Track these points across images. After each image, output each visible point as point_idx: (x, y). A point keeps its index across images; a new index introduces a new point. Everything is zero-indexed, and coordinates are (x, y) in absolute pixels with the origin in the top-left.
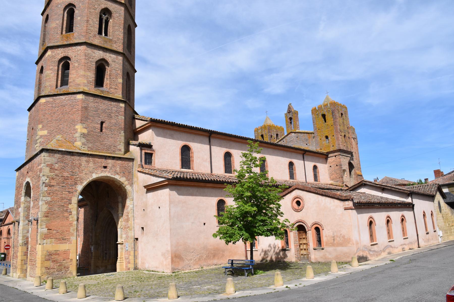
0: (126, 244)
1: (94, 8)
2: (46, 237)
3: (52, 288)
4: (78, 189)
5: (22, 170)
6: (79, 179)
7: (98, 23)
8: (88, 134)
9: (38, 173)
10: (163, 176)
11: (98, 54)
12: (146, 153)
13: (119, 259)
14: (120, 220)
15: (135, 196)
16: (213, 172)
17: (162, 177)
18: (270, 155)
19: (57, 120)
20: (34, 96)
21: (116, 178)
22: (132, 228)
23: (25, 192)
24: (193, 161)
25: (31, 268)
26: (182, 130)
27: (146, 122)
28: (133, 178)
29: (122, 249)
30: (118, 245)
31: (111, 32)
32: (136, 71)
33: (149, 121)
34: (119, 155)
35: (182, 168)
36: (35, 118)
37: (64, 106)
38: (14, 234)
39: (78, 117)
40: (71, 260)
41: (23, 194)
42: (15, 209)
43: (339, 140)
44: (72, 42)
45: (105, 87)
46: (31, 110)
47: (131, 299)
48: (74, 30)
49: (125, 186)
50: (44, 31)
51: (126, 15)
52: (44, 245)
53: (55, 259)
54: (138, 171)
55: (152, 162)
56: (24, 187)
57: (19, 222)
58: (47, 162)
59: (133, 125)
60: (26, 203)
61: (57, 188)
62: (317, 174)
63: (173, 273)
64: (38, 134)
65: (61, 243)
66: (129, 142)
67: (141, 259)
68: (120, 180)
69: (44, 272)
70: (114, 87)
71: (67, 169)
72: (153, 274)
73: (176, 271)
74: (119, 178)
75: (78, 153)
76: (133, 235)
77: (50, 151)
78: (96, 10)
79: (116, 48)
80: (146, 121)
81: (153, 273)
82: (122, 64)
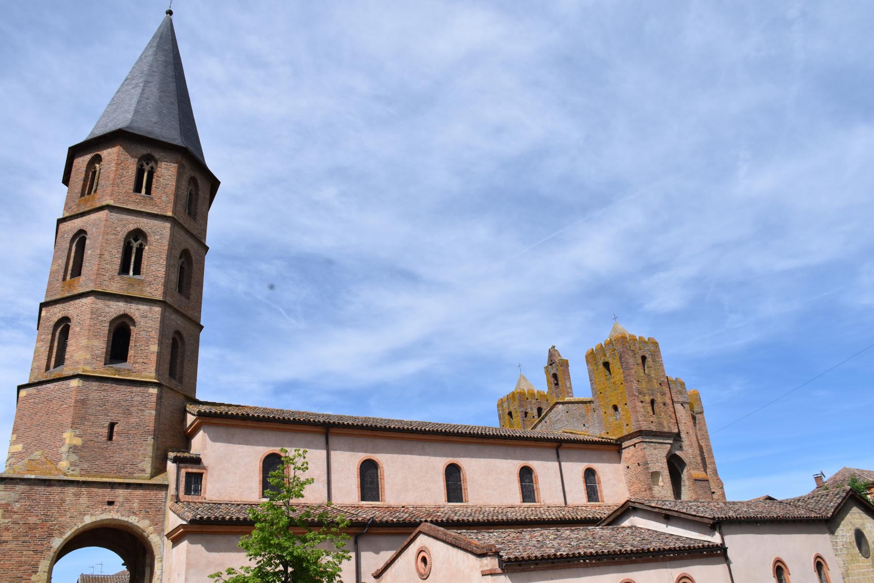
1: (115, 232)
6: (57, 527)
8: (83, 446)
12: (188, 474)
16: (334, 501)
18: (472, 457)
21: (130, 521)
26: (263, 426)
32: (202, 327)
34: (141, 479)
37: (51, 401)
39: (68, 418)
43: (637, 412)
44: (76, 292)
49: (148, 536)
51: (175, 234)
62: (597, 485)
70: (142, 360)
71: (36, 510)
77: (6, 481)
78: (118, 235)
79: (151, 293)
82: (159, 319)
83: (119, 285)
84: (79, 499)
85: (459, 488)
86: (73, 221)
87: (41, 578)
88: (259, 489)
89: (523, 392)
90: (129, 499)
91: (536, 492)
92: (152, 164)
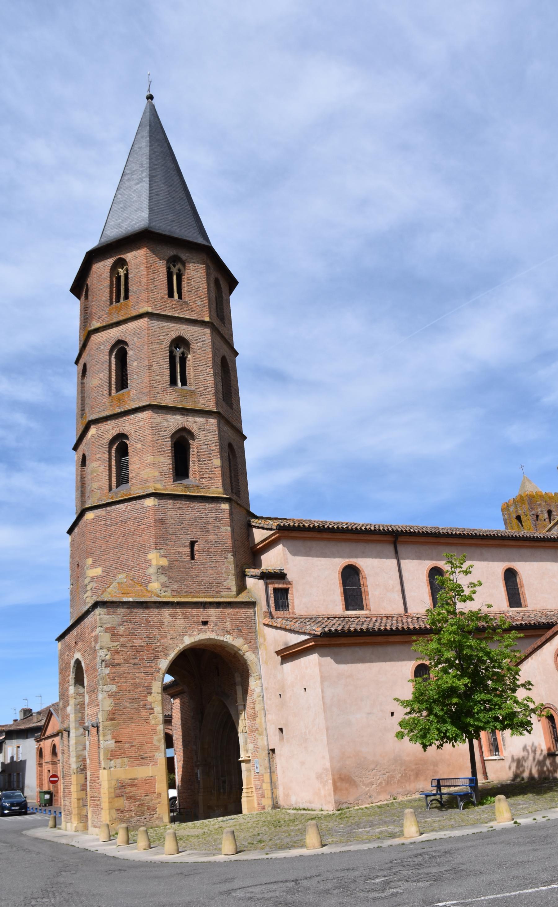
0: (254, 761)
1: (159, 341)
2: (113, 755)
3: (128, 842)
4: (161, 666)
5: (67, 638)
6: (160, 649)
7: (167, 366)
8: (170, 567)
9: (93, 644)
10: (306, 631)
11: (173, 420)
12: (275, 589)
13: (244, 791)
14: (242, 717)
15: (263, 670)
16: (409, 611)
17: (304, 634)
18: (526, 561)
19: (116, 548)
20: (76, 507)
21: (225, 640)
22: (262, 732)
23: (75, 678)
24: (367, 593)
25: (94, 812)
27: (271, 532)
28: (256, 639)
29: (249, 770)
30: (242, 764)
31: (192, 376)
32: (245, 438)
33: (275, 530)
34: (228, 597)
35: (347, 609)
36: (80, 546)
38: (63, 753)
39: (149, 538)
40: (159, 794)
41: (72, 681)
42: (61, 709)
44: (128, 407)
45: (193, 479)
46: (73, 533)
47: (248, 852)
48: (129, 385)
49: (244, 654)
50: (82, 392)
52: (112, 769)
53: (131, 794)
54: (265, 625)
55: (288, 604)
56: (73, 669)
57: (69, 732)
58: (105, 623)
59: (250, 539)
60: (78, 697)
61: (124, 668)
63: (339, 810)
64: (86, 575)
65: (139, 765)
66: (245, 572)
67: (284, 789)
68: (234, 644)
69: (114, 817)
70: (208, 475)
71: (139, 633)
72: (302, 815)
73: (344, 806)
74: (231, 639)
75: (155, 603)
76: (266, 744)
77: (108, 604)
78: (162, 344)
79: (204, 404)
80: (271, 529)
81: (303, 812)
83: (172, 397)
84: (176, 621)
85: (517, 593)
86: (107, 331)
87: (156, 699)
88: (342, 601)
89: (532, 494)
90: (221, 618)
91: (521, 596)
92: (179, 266)
